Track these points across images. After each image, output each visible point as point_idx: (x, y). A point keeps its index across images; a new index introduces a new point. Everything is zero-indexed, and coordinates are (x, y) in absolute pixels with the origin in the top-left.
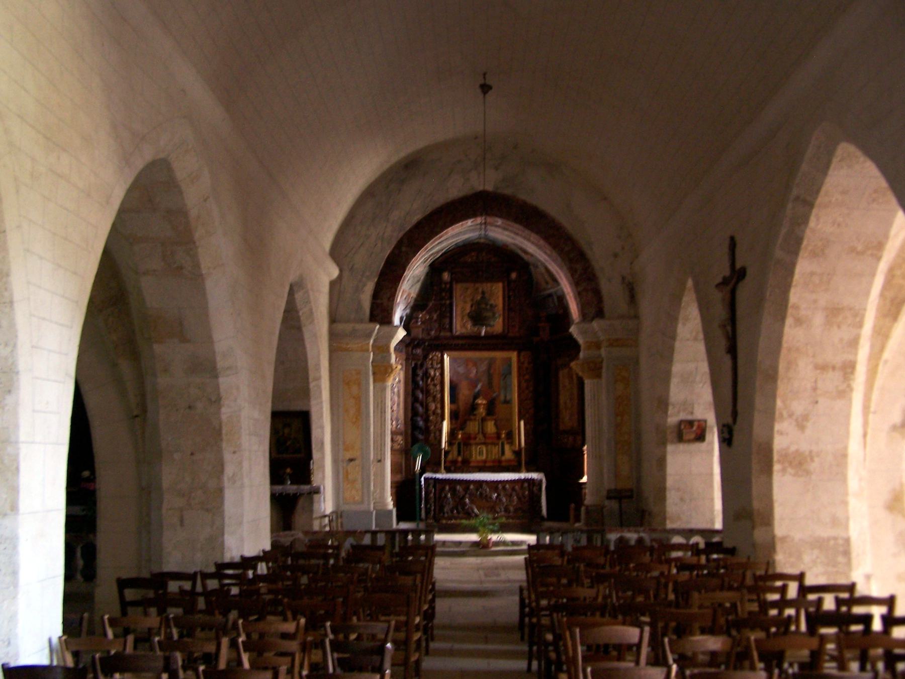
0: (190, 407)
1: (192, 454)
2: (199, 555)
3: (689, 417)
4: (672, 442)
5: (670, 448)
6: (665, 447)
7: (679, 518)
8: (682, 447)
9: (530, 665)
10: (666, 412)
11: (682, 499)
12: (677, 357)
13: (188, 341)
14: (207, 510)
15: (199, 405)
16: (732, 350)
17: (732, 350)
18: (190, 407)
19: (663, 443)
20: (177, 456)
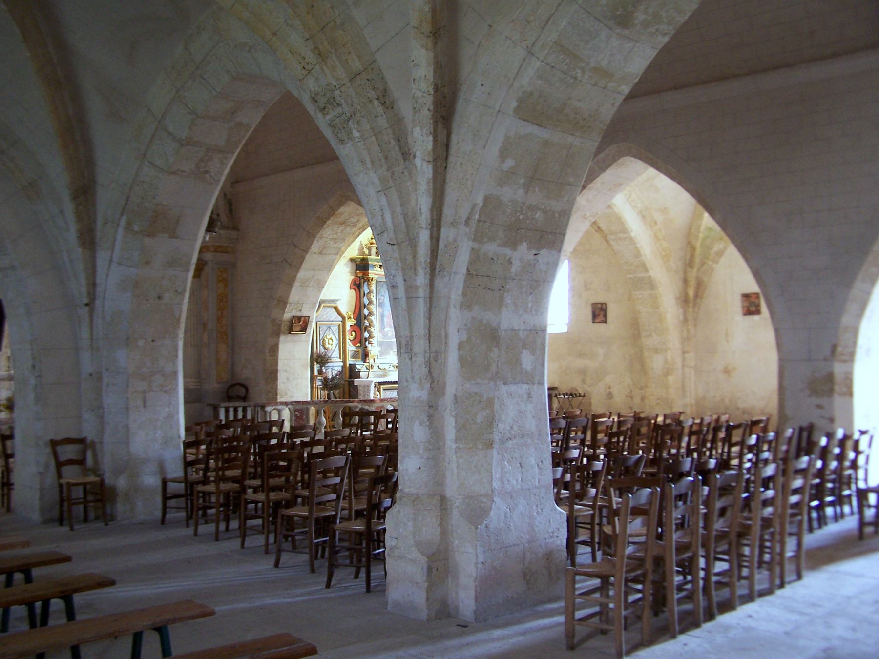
0: (159, 298)
1: (153, 341)
2: (159, 432)
3: (299, 314)
4: (284, 334)
5: (282, 338)
6: (279, 338)
7: (286, 394)
8: (290, 337)
9: (217, 528)
10: (284, 309)
11: (288, 379)
12: (304, 265)
13: (177, 238)
14: (166, 392)
15: (167, 296)
16: (430, 319)
17: (430, 319)
18: (159, 298)
19: (277, 334)
20: (141, 343)
